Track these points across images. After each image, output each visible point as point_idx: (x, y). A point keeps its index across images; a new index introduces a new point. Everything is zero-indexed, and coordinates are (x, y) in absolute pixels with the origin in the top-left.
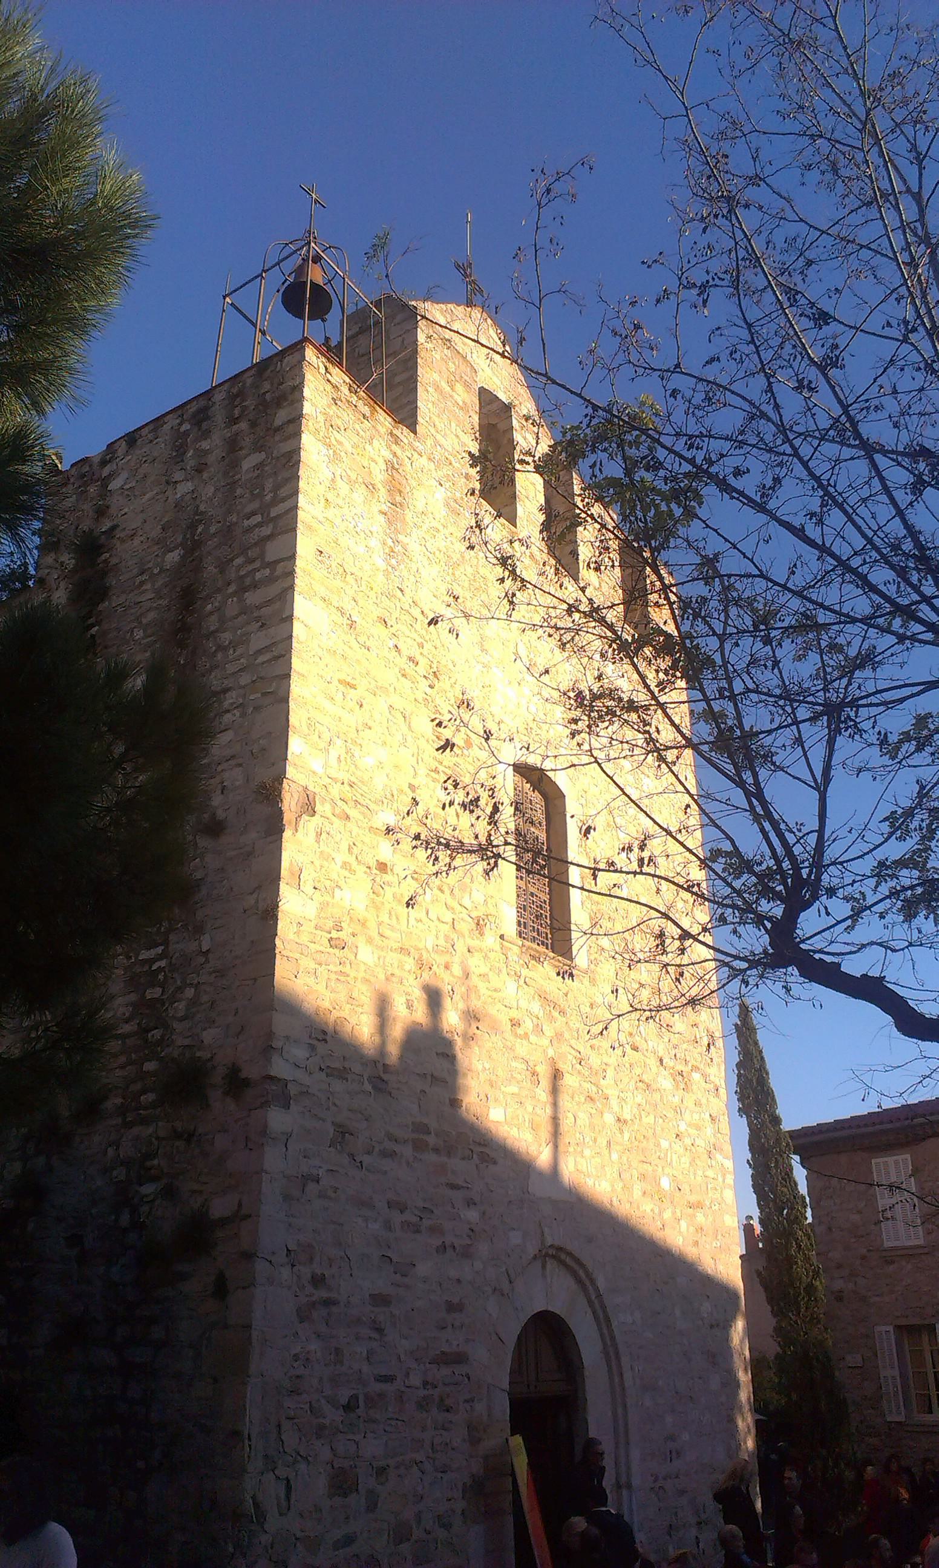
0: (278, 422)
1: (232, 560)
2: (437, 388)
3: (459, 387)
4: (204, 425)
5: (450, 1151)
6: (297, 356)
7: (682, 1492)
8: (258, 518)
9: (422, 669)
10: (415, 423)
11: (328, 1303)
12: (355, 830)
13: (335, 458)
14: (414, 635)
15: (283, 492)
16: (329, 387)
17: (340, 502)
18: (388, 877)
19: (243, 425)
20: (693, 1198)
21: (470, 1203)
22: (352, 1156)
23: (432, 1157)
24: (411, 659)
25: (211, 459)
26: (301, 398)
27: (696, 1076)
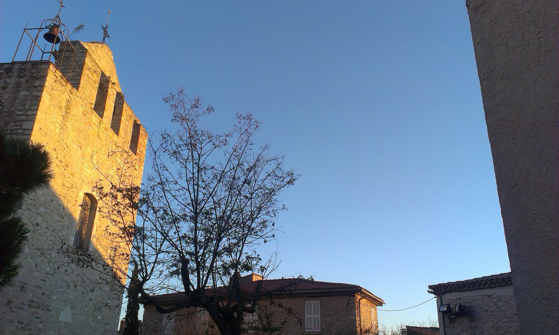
0: (36, 85)
1: (10, 123)
2: (88, 76)
3: (95, 75)
4: (9, 74)
5: (38, 308)
6: (46, 66)
8: (22, 113)
9: (63, 164)
10: (78, 87)
12: (32, 213)
13: (52, 99)
14: (63, 154)
15: (33, 108)
16: (55, 77)
17: (50, 113)
18: (39, 228)
19: (23, 80)
21: (41, 322)
22: (10, 308)
23: (34, 309)
24: (60, 161)
25: (9, 86)
26: (45, 80)
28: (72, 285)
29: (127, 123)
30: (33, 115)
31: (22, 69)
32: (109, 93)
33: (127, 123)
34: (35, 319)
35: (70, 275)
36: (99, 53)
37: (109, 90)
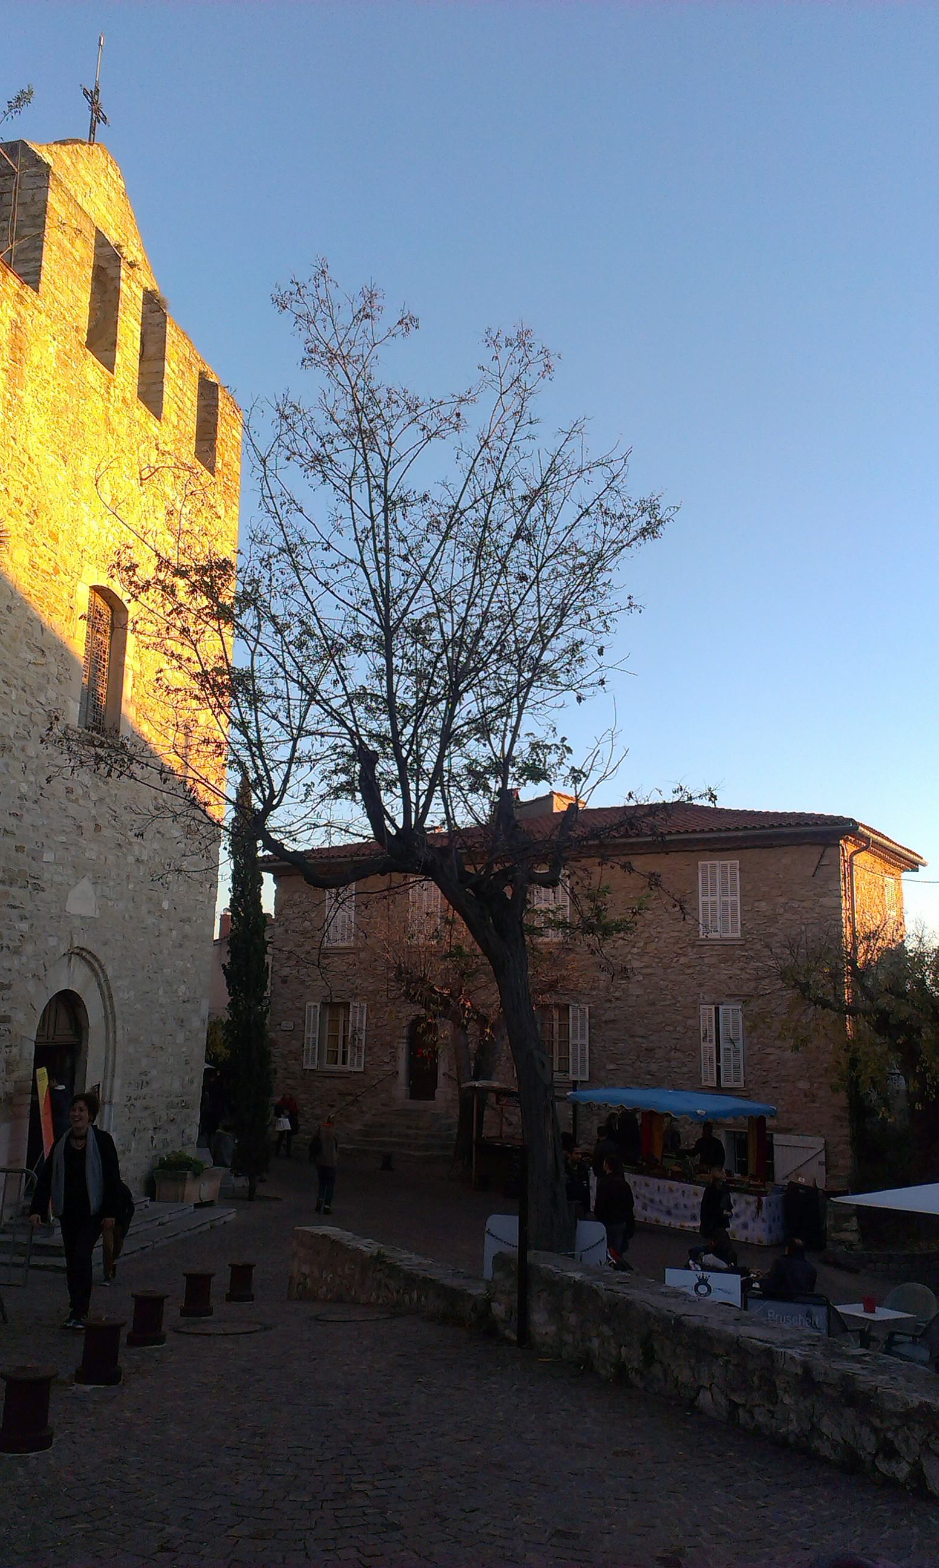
21: (23, 918)
32: (122, 296)
35: (81, 802)
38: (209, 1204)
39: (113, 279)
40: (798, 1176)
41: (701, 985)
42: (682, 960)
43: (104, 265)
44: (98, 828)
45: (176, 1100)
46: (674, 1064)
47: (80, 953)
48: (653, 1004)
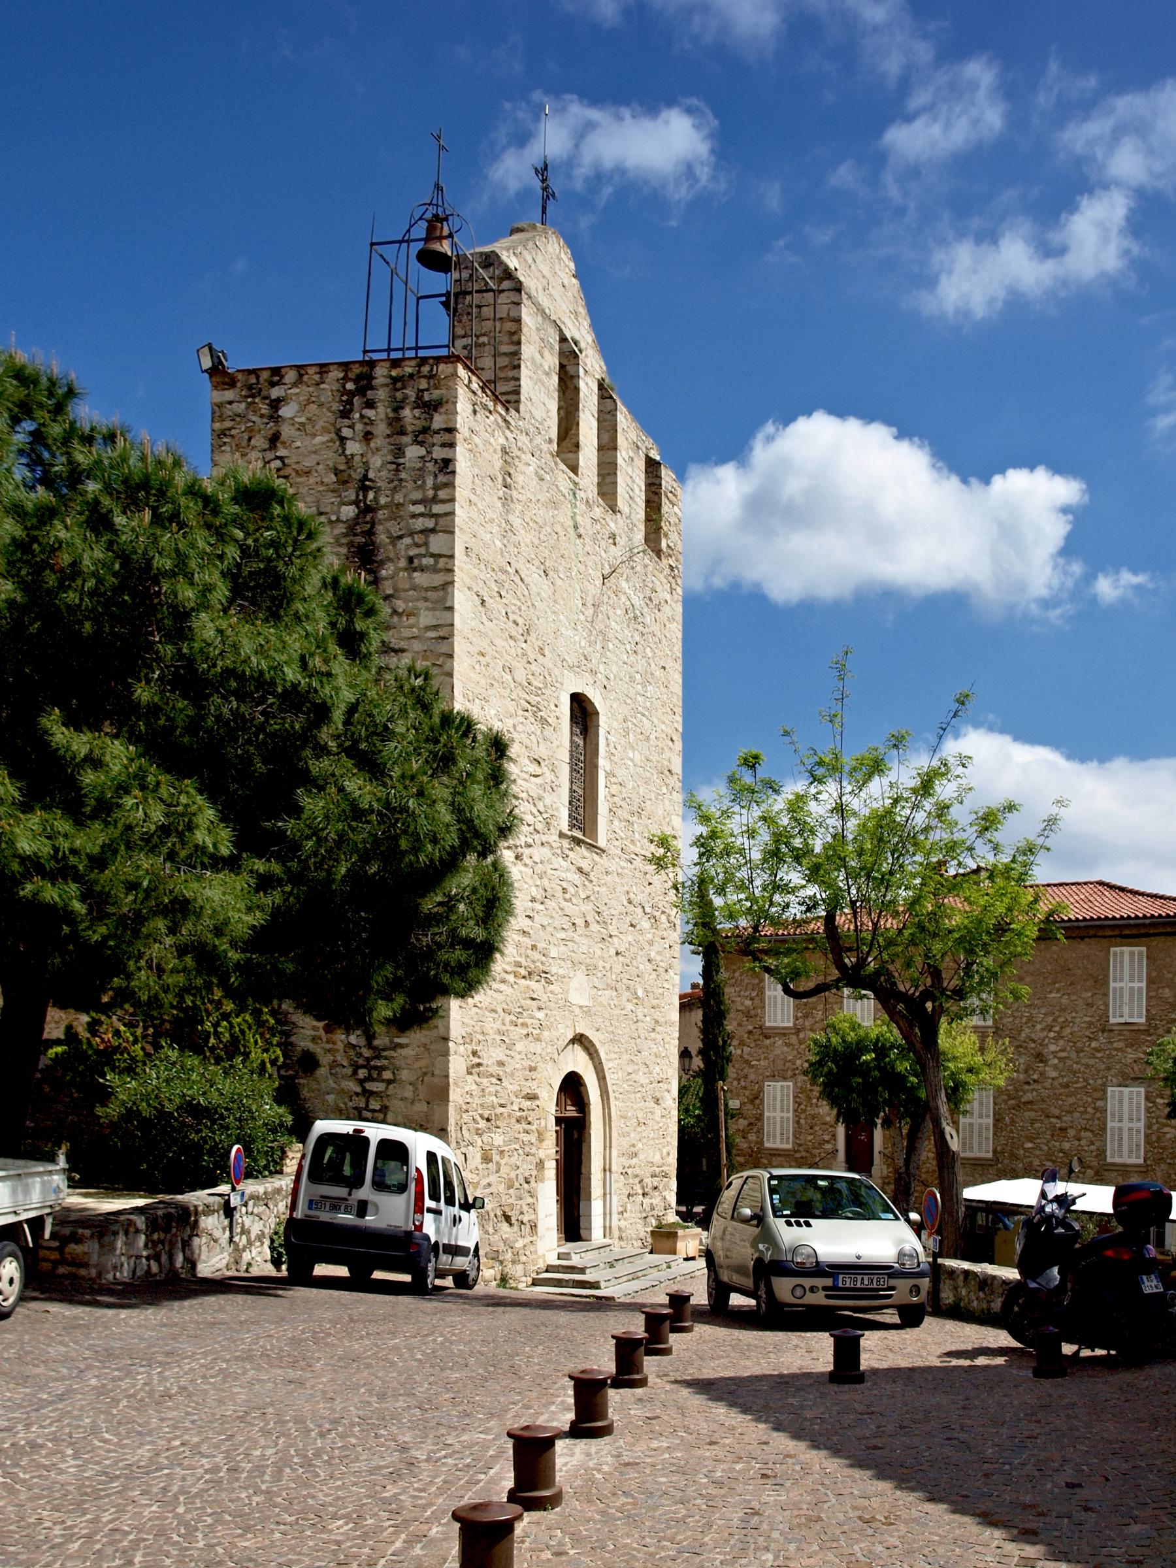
1: (401, 537)
7: (637, 1176)
11: (479, 1065)
15: (442, 494)
20: (655, 1002)
21: (540, 1009)
27: (664, 917)
28: (580, 922)
29: (630, 470)
30: (446, 514)
31: (395, 380)
32: (581, 395)
33: (630, 470)
34: (530, 1002)
35: (574, 901)
36: (541, 266)
37: (582, 385)
38: (693, 1259)
39: (572, 377)
40: (1077, 1220)
41: (1109, 1069)
42: (1094, 1044)
43: (565, 363)
44: (587, 923)
45: (658, 1170)
46: (1083, 1142)
47: (580, 1040)
48: (1066, 1086)
